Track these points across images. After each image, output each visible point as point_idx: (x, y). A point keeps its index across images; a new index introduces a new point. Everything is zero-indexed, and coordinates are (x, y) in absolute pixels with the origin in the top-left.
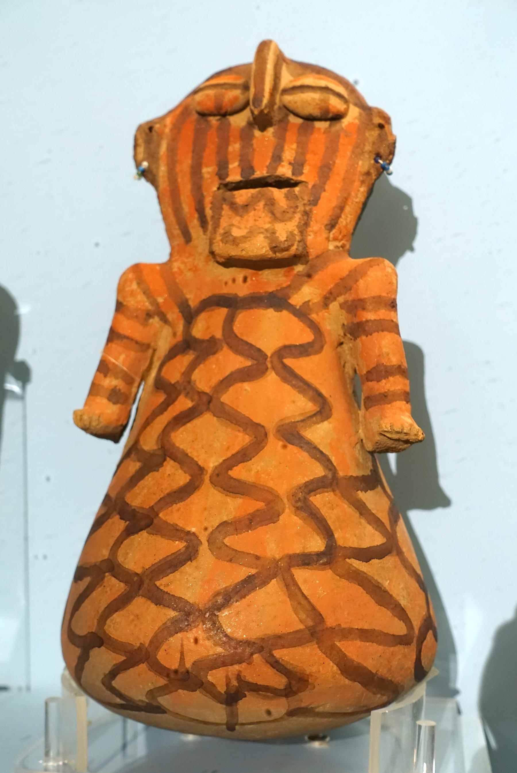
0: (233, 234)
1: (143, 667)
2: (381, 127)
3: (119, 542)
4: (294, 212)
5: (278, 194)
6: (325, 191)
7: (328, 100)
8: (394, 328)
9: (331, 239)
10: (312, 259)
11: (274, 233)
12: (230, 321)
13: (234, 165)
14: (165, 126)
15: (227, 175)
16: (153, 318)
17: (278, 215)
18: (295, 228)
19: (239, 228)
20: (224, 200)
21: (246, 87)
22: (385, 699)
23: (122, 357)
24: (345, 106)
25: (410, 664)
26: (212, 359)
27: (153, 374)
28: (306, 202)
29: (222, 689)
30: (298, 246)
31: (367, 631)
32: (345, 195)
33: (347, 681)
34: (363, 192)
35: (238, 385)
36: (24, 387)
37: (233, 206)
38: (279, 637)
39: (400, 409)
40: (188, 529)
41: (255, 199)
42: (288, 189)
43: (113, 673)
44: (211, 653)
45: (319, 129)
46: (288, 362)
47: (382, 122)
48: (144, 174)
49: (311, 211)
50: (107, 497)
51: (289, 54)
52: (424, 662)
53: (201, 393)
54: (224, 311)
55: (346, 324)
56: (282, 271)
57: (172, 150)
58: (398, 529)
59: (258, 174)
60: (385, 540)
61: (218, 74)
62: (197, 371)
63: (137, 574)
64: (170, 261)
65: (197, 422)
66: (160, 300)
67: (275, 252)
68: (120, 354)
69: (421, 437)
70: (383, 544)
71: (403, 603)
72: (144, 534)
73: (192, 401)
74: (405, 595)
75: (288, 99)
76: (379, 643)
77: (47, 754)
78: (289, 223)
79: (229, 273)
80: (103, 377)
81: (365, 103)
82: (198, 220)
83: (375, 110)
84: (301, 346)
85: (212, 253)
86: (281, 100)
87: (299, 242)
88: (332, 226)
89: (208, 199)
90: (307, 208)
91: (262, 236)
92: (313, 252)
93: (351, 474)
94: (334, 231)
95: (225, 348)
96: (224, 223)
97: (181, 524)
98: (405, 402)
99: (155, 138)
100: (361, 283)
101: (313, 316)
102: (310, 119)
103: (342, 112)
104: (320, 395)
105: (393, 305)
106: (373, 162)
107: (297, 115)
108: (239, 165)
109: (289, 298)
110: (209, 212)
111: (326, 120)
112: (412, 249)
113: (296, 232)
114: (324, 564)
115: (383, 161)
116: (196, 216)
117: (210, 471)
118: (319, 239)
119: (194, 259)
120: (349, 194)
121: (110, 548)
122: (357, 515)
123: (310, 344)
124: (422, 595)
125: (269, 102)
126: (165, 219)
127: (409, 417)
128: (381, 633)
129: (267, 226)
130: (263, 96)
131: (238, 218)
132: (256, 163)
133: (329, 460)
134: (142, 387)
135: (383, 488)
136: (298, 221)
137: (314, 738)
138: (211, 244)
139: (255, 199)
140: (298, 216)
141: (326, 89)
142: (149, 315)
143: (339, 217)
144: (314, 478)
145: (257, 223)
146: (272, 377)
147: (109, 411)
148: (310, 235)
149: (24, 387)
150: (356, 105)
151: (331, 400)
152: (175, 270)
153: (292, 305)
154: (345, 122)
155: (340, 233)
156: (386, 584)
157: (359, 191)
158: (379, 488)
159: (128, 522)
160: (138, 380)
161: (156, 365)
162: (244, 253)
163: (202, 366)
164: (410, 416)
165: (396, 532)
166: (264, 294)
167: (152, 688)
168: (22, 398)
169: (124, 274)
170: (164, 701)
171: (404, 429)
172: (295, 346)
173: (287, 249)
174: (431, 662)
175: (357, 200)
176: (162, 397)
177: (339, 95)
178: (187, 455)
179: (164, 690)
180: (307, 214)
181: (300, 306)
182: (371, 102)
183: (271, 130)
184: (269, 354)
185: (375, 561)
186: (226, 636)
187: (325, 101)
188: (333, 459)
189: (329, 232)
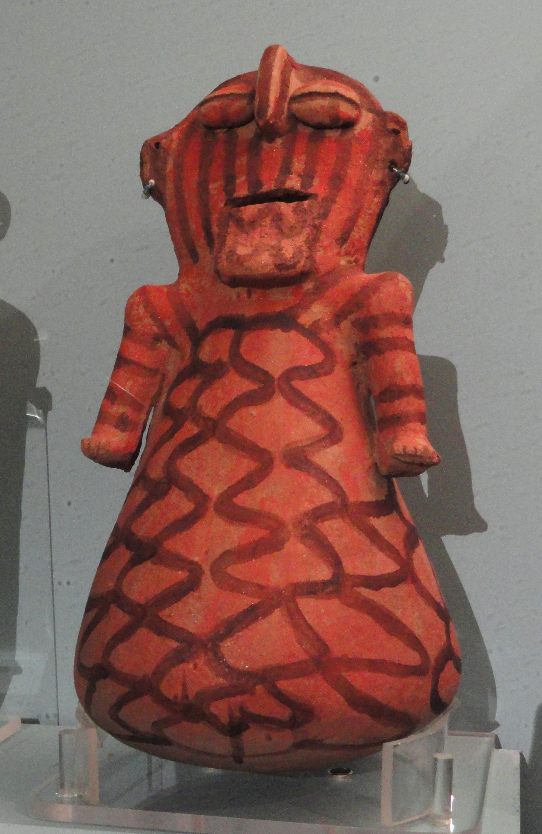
0: (237, 252)
1: (147, 699)
2: (396, 132)
3: (124, 572)
4: (302, 227)
5: (286, 208)
6: (335, 202)
7: (338, 106)
8: (410, 346)
9: (342, 253)
10: (323, 276)
11: (280, 249)
12: (236, 343)
13: (241, 179)
14: (172, 141)
15: (234, 191)
16: (161, 342)
17: (286, 231)
18: (302, 244)
19: (245, 246)
20: (230, 216)
21: (251, 96)
22: (398, 732)
23: (129, 383)
24: (356, 112)
25: (425, 695)
26: (217, 384)
27: (163, 400)
28: (315, 215)
29: (225, 719)
30: (305, 262)
31: (373, 661)
32: (357, 207)
33: (355, 713)
34: (377, 203)
35: (243, 411)
36: (45, 415)
37: (239, 223)
38: (280, 667)
39: (415, 431)
40: (192, 558)
41: (261, 215)
42: (297, 202)
43: (119, 705)
44: (213, 684)
45: (330, 138)
46: (297, 384)
47: (395, 127)
48: (151, 192)
49: (320, 225)
50: (116, 528)
51: (300, 59)
52: (443, 693)
53: (207, 419)
54: (231, 333)
55: (358, 343)
56: (289, 290)
57: (179, 166)
58: (415, 556)
59: (265, 188)
60: (399, 567)
61: (226, 84)
62: (203, 396)
63: (140, 605)
64: (178, 283)
65: (203, 449)
66: (168, 323)
67: (280, 270)
68: (127, 380)
69: (436, 460)
70: (396, 572)
71: (418, 631)
72: (148, 564)
73: (198, 426)
74: (420, 624)
75: (296, 106)
76: (390, 674)
77: (62, 785)
78: (296, 238)
79: (233, 293)
80: (109, 406)
81: (380, 107)
82: (205, 239)
83: (390, 115)
84: (310, 367)
85: (217, 272)
86: (289, 110)
87: (307, 258)
88: (344, 238)
89: (215, 216)
90: (317, 222)
91: (267, 253)
92: (322, 269)
93: (362, 500)
94: (345, 245)
95: (232, 372)
96: (229, 242)
97: (183, 552)
98: (419, 424)
99: (162, 155)
100: (374, 299)
101: (324, 335)
102: (320, 128)
103: (354, 119)
104: (330, 418)
105: (407, 322)
106: (387, 170)
107: (306, 124)
108: (246, 180)
109: (298, 317)
110: (215, 229)
111: (337, 128)
112: (443, 260)
113: (304, 248)
114: (331, 593)
115: (398, 169)
116: (203, 234)
117: (214, 499)
118: (329, 254)
119: (201, 280)
120: (362, 206)
121: (115, 579)
122: (368, 542)
123: (321, 365)
124: (441, 623)
125: (274, 112)
126: (173, 239)
127: (424, 439)
128: (393, 664)
129: (273, 243)
130: (268, 106)
131: (244, 236)
132: (264, 177)
133: (337, 485)
134: (151, 414)
135: (400, 513)
136: (306, 236)
137: (336, 772)
138: (217, 263)
139: (261, 215)
140: (307, 230)
141: (336, 95)
142: (157, 339)
143: (351, 230)
144: (321, 505)
145: (263, 240)
146: (279, 400)
147: (116, 439)
148: (319, 251)
149: (45, 415)
150: (370, 110)
151: (343, 424)
152: (183, 291)
153: (302, 325)
154: (358, 128)
155: (353, 247)
156: (398, 614)
157: (372, 201)
158: (395, 513)
159: (133, 553)
160: (147, 405)
161: (166, 390)
162: (248, 272)
163: (208, 391)
164: (426, 438)
165: (412, 560)
166: (271, 314)
167: (156, 720)
168: (44, 426)
169: (132, 297)
170: (170, 732)
171: (417, 452)
172: (304, 368)
173: (294, 266)
174: (452, 694)
175: (370, 212)
176: (169, 424)
177: (350, 101)
178: (192, 482)
179: (168, 722)
180: (317, 228)
181: (310, 326)
182: (387, 106)
183: (279, 141)
184: (276, 376)
185: (386, 590)
186: (229, 667)
187: (335, 108)
188: (342, 484)
189: (341, 247)
